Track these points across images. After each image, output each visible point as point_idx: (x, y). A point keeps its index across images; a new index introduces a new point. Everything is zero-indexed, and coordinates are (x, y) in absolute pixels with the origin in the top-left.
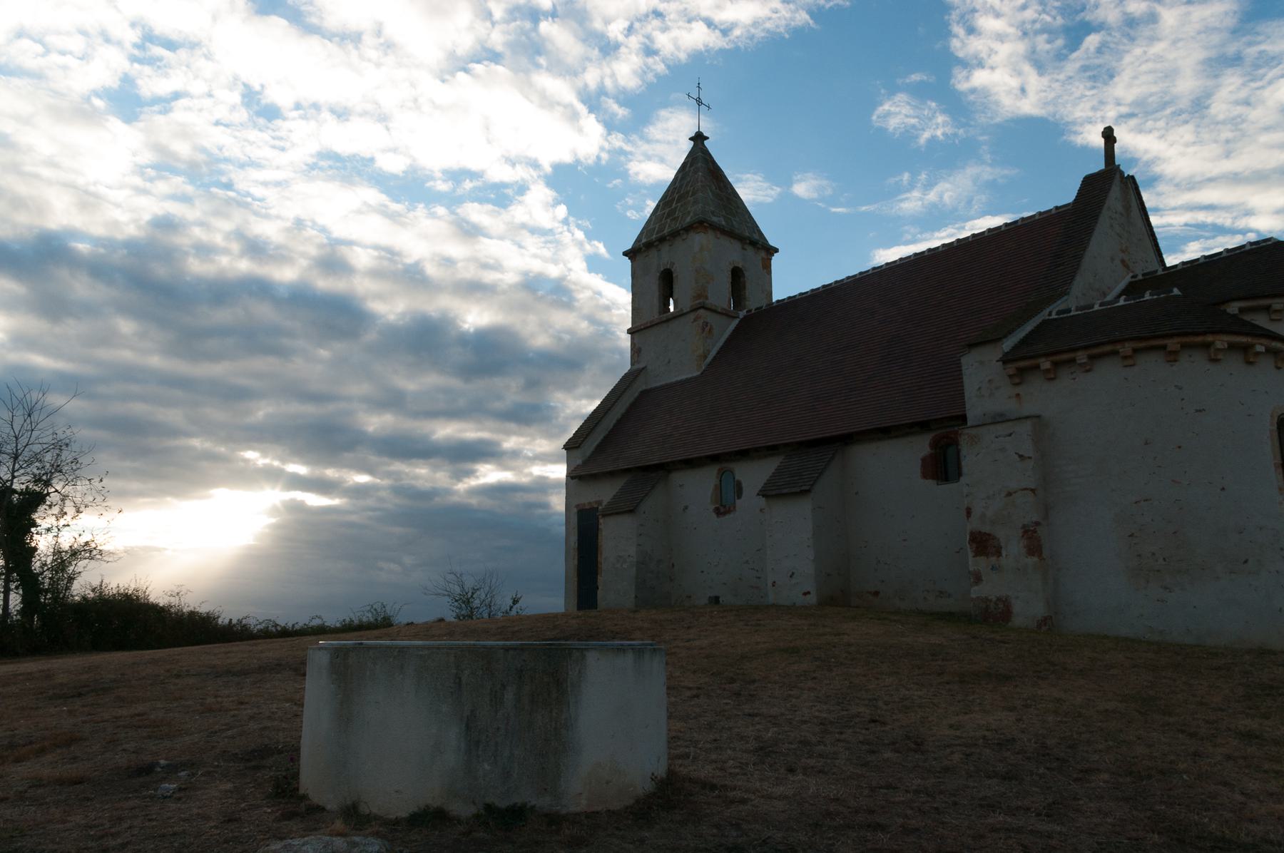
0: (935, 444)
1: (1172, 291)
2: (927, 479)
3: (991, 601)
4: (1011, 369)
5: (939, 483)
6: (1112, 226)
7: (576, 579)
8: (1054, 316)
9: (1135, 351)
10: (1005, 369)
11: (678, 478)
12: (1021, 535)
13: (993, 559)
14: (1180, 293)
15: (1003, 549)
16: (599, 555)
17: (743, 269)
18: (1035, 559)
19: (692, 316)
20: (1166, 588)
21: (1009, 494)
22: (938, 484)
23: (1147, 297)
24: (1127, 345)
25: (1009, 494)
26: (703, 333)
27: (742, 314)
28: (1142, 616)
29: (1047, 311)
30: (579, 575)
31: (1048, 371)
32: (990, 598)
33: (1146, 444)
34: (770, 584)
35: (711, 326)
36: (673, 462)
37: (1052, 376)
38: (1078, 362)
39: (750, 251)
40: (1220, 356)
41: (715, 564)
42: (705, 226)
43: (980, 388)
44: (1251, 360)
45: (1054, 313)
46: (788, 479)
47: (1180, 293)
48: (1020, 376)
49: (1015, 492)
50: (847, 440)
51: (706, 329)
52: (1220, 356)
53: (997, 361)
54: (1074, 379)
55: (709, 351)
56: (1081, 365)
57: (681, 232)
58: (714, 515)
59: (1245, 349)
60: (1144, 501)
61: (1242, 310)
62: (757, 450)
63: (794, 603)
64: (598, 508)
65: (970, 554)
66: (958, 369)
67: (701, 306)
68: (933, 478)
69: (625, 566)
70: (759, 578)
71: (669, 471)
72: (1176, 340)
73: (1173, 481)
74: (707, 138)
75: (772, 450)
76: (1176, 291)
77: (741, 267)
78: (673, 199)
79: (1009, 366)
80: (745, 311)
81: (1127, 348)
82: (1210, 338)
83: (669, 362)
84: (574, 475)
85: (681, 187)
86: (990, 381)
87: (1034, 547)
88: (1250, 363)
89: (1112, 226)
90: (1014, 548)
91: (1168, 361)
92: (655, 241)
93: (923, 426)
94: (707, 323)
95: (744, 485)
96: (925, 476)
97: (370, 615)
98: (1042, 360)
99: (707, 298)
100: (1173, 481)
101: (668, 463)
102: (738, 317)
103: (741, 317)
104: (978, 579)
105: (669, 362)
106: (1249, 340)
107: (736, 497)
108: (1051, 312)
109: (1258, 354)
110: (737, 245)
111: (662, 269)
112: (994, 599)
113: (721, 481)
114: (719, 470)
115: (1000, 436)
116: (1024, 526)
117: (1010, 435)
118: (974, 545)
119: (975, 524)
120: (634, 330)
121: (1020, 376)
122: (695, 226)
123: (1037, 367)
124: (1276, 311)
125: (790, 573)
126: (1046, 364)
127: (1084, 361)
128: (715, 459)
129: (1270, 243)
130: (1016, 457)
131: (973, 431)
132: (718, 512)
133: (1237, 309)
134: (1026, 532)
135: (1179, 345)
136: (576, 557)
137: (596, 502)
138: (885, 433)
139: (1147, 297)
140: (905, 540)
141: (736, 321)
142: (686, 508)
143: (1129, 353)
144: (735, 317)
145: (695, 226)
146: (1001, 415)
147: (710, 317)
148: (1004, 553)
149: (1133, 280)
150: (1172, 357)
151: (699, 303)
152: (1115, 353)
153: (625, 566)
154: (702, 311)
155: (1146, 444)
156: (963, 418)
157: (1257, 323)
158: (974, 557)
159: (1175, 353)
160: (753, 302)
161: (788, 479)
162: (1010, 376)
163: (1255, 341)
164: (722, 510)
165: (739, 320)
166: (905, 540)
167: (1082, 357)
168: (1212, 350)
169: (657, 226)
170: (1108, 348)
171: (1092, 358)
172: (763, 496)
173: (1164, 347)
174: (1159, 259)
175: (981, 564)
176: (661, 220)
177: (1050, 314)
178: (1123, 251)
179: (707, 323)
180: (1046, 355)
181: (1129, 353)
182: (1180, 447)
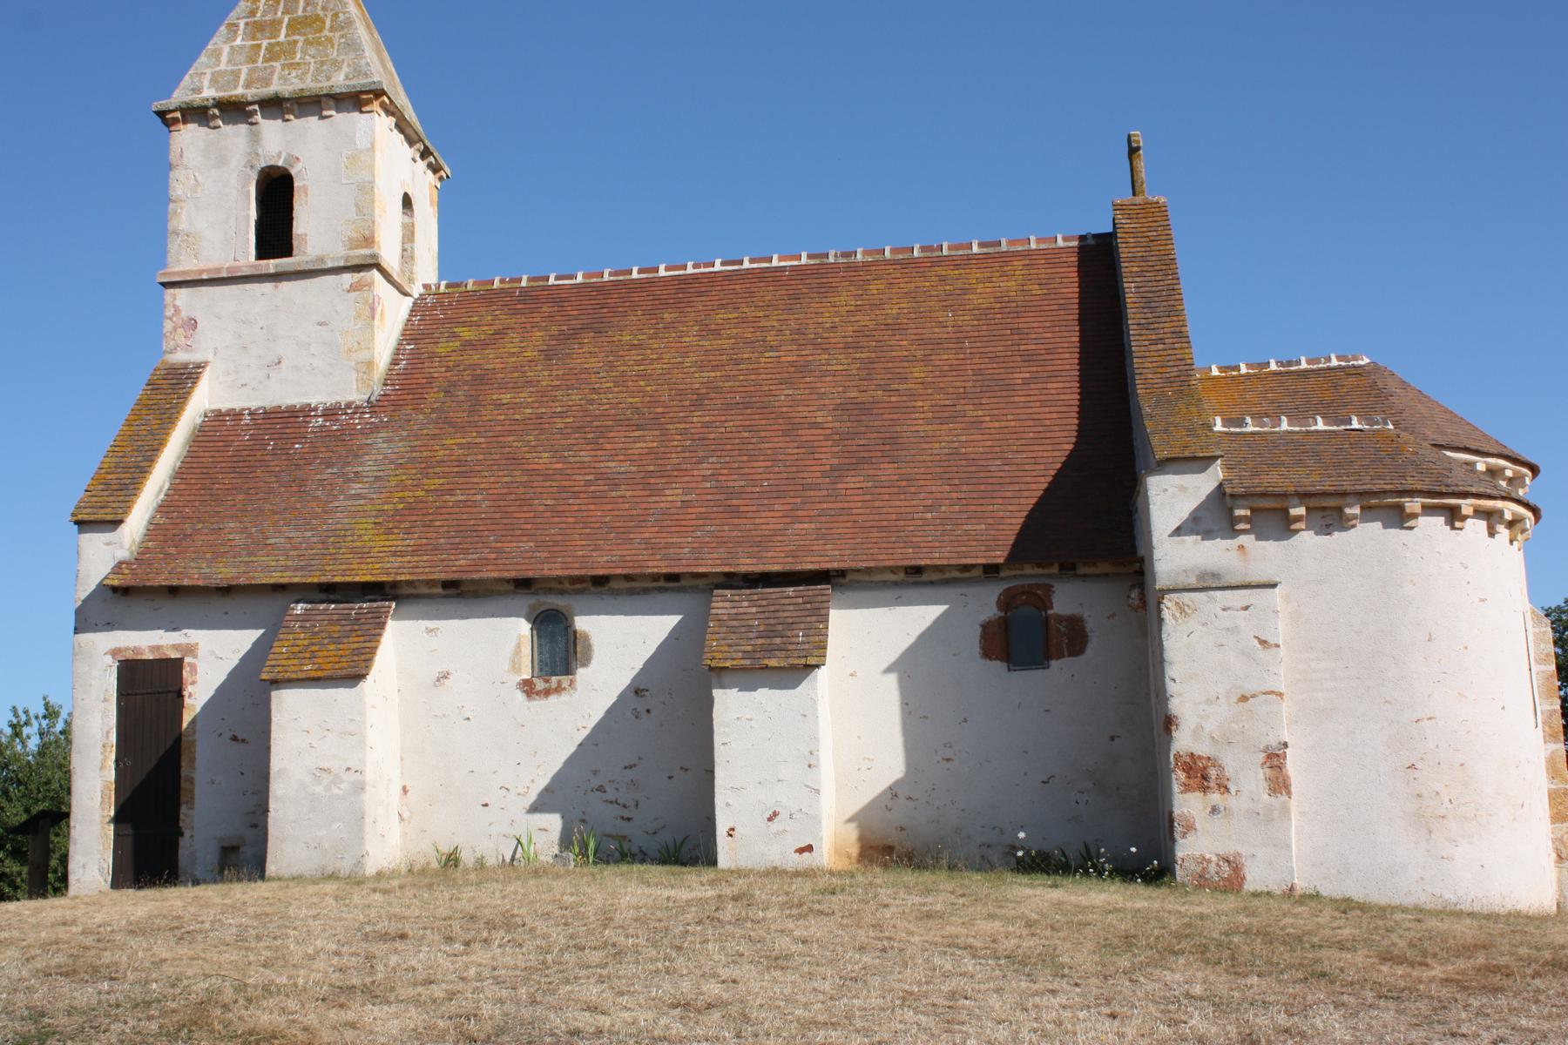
0: (1006, 602)
2: (991, 659)
3: (1209, 861)
5: (1011, 668)
12: (1262, 761)
16: (184, 764)
19: (348, 278)
21: (1244, 699)
22: (1009, 670)
25: (1244, 699)
32: (1207, 856)
49: (1253, 696)
57: (324, 99)
60: (1428, 719)
63: (1292, 889)
68: (1001, 659)
70: (629, 819)
84: (116, 583)
111: (263, 165)
120: (1130, 270)
125: (771, 812)
130: (1256, 642)
134: (1269, 757)
140: (948, 760)
146: (1214, 575)
166: (948, 760)
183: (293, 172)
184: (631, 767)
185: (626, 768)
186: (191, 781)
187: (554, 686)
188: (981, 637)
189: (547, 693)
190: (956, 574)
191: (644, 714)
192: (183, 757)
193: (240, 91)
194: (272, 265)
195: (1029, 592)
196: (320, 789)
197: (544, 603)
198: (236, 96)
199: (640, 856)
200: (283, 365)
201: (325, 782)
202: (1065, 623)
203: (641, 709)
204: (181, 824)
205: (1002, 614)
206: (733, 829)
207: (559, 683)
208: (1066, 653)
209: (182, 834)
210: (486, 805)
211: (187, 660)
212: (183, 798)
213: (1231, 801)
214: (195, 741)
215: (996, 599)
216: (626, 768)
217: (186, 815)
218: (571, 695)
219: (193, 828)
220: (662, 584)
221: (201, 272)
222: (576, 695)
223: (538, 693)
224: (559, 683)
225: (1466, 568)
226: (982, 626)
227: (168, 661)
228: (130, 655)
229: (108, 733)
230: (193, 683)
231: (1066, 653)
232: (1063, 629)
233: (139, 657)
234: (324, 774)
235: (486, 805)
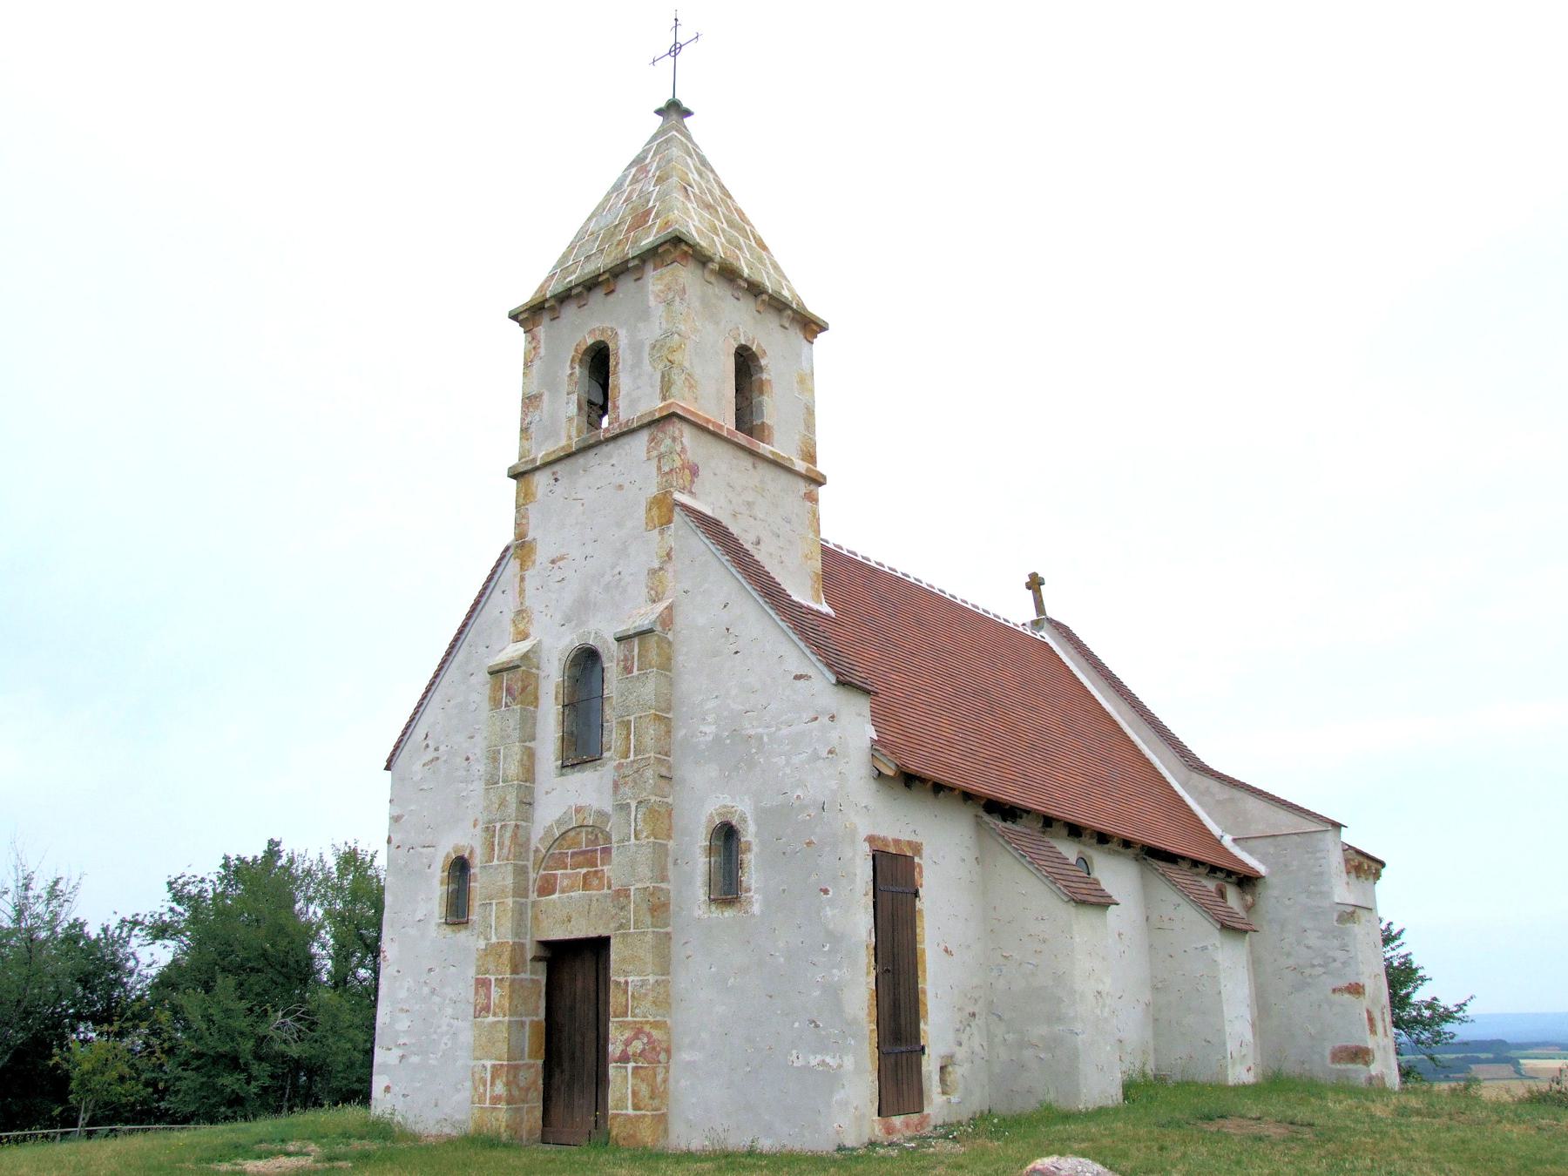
74: (688, 113)
137: (909, 843)
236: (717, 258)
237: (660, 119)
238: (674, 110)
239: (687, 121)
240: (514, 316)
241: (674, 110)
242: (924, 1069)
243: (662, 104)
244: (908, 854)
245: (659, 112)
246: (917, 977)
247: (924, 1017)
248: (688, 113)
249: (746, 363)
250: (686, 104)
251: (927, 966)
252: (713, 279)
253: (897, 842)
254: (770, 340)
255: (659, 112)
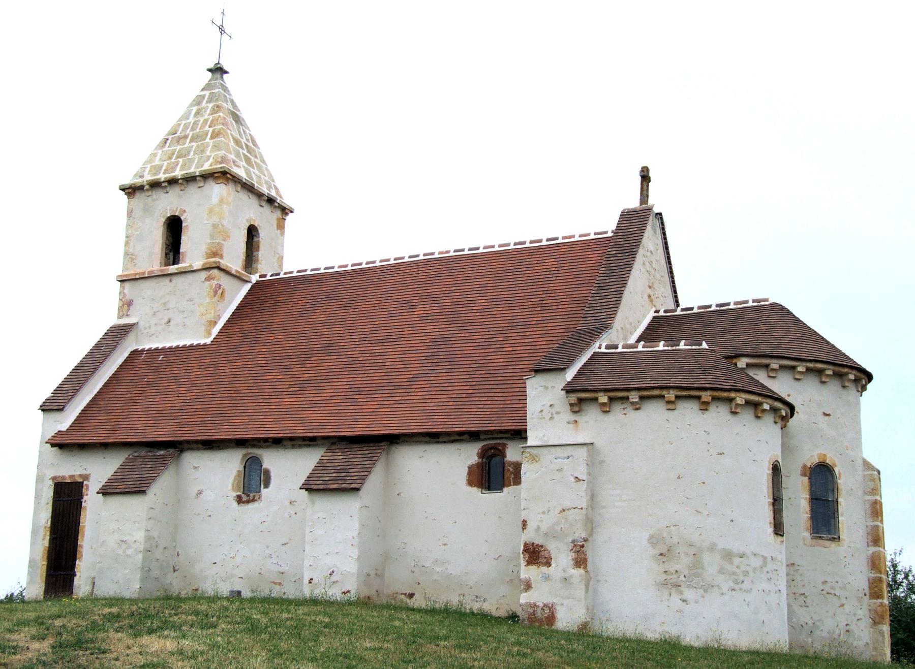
0: (483, 454)
1: (701, 345)
3: (538, 607)
4: (573, 398)
5: (484, 492)
6: (644, 264)
7: (45, 563)
8: (603, 350)
9: (677, 397)
10: (567, 397)
11: (191, 459)
13: (544, 569)
14: (707, 347)
15: (553, 560)
17: (259, 228)
18: (582, 571)
19: (204, 275)
20: (684, 601)
23: (682, 346)
24: (672, 392)
26: (215, 296)
27: (255, 278)
28: (663, 623)
29: (597, 344)
30: (49, 559)
31: (604, 404)
32: (538, 604)
33: (679, 477)
34: (306, 581)
35: (223, 289)
36: (188, 442)
37: (608, 410)
38: (631, 400)
39: (267, 209)
40: (738, 410)
41: (232, 556)
42: (227, 177)
43: (542, 411)
44: (759, 415)
45: (603, 346)
46: (334, 475)
47: (707, 347)
48: (578, 406)
49: (568, 509)
50: (394, 440)
51: (219, 293)
52: (738, 410)
53: (562, 390)
54: (625, 414)
55: (219, 317)
56: (632, 403)
57: (198, 178)
58: (235, 504)
59: (756, 405)
61: (748, 365)
62: (291, 439)
64: (83, 482)
65: (523, 563)
66: (522, 390)
67: (214, 268)
68: (478, 487)
69: (129, 552)
71: (182, 451)
72: (709, 393)
73: (696, 511)
74: (226, 72)
75: (309, 441)
76: (705, 345)
77: (256, 225)
78: (186, 137)
79: (572, 395)
80: (257, 275)
81: (671, 395)
82: (733, 395)
83: (169, 321)
85: (196, 123)
86: (551, 405)
87: (581, 562)
88: (758, 417)
89: (644, 264)
90: (562, 559)
91: (701, 410)
92: (164, 182)
93: (473, 436)
94: (220, 285)
95: (273, 475)
96: (470, 483)
97: (213, 593)
98: (601, 394)
99: (221, 257)
100: (696, 511)
101: (181, 442)
102: (250, 282)
103: (254, 281)
104: (528, 586)
105: (169, 321)
106: (760, 399)
107: (262, 486)
108: (600, 346)
109: (765, 410)
110: (254, 201)
111: (169, 215)
112: (541, 605)
113: (245, 467)
114: (245, 456)
115: (559, 458)
116: (573, 542)
117: (569, 457)
118: (527, 556)
119: (530, 536)
121: (578, 406)
122: (216, 175)
123: (596, 399)
124: (773, 370)
125: (331, 571)
126: (603, 399)
127: (637, 400)
128: (240, 443)
129: (767, 303)
131: (534, 451)
132: (239, 500)
133: (745, 363)
135: (710, 398)
136: (48, 538)
137: (81, 476)
138: (434, 438)
139: (682, 346)
140: (445, 545)
141: (246, 288)
142: (200, 492)
143: (673, 399)
144: (247, 281)
145: (216, 175)
147: (225, 281)
148: (553, 563)
149: (656, 314)
150: (705, 406)
151: (215, 262)
152: (662, 397)
153: (129, 552)
154: (215, 272)
155: (679, 477)
156: (520, 434)
157: (756, 377)
158: (526, 566)
159: (707, 404)
160: (266, 268)
161: (334, 475)
162: (571, 405)
163: (764, 400)
164: (245, 498)
165: (251, 284)
166: (445, 545)
167: (634, 397)
168: (733, 404)
169: (165, 163)
170: (656, 392)
171: (642, 398)
172: (307, 490)
173: (699, 398)
174: (674, 295)
175: (528, 572)
176: (170, 158)
177: (600, 348)
178: (650, 287)
179: (220, 285)
180: (606, 391)
181: (673, 399)
182: (704, 483)
183: (182, 218)
184: (285, 544)
185: (283, 545)
186: (81, 546)
187: (251, 498)
188: (468, 474)
189: (248, 502)
190: (457, 437)
191: (293, 515)
192: (79, 534)
193: (192, 170)
194: (173, 269)
195: (494, 447)
196: (121, 552)
197: (251, 453)
198: (190, 173)
199: (572, 637)
200: (171, 323)
201: (124, 548)
202: (512, 466)
203: (293, 512)
204: (76, 570)
205: (480, 461)
206: (311, 579)
207: (254, 497)
208: (512, 484)
209: (75, 575)
210: (215, 563)
211: (85, 483)
212: (47, 549)
213: (551, 570)
214: (85, 526)
215: (477, 452)
216: (283, 545)
217: (78, 565)
218: (259, 504)
219: (81, 572)
220: (308, 442)
221: (136, 274)
222: (262, 504)
223: (244, 502)
224: (254, 497)
225: (708, 434)
226: (469, 468)
227: (76, 483)
228: (60, 480)
229: (48, 521)
230: (87, 495)
231: (512, 484)
232: (511, 470)
233: (64, 481)
234: (123, 544)
235: (215, 563)
236: (145, 183)
237: (210, 74)
238: (218, 70)
239: (225, 76)
240: (123, 189)
241: (218, 70)
242: (75, 583)
243: (211, 66)
244: (79, 481)
245: (210, 70)
246: (78, 539)
247: (79, 558)
248: (226, 72)
249: (252, 232)
250: (225, 68)
251: (86, 534)
252: (150, 193)
253: (71, 477)
254: (264, 218)
255: (210, 70)
